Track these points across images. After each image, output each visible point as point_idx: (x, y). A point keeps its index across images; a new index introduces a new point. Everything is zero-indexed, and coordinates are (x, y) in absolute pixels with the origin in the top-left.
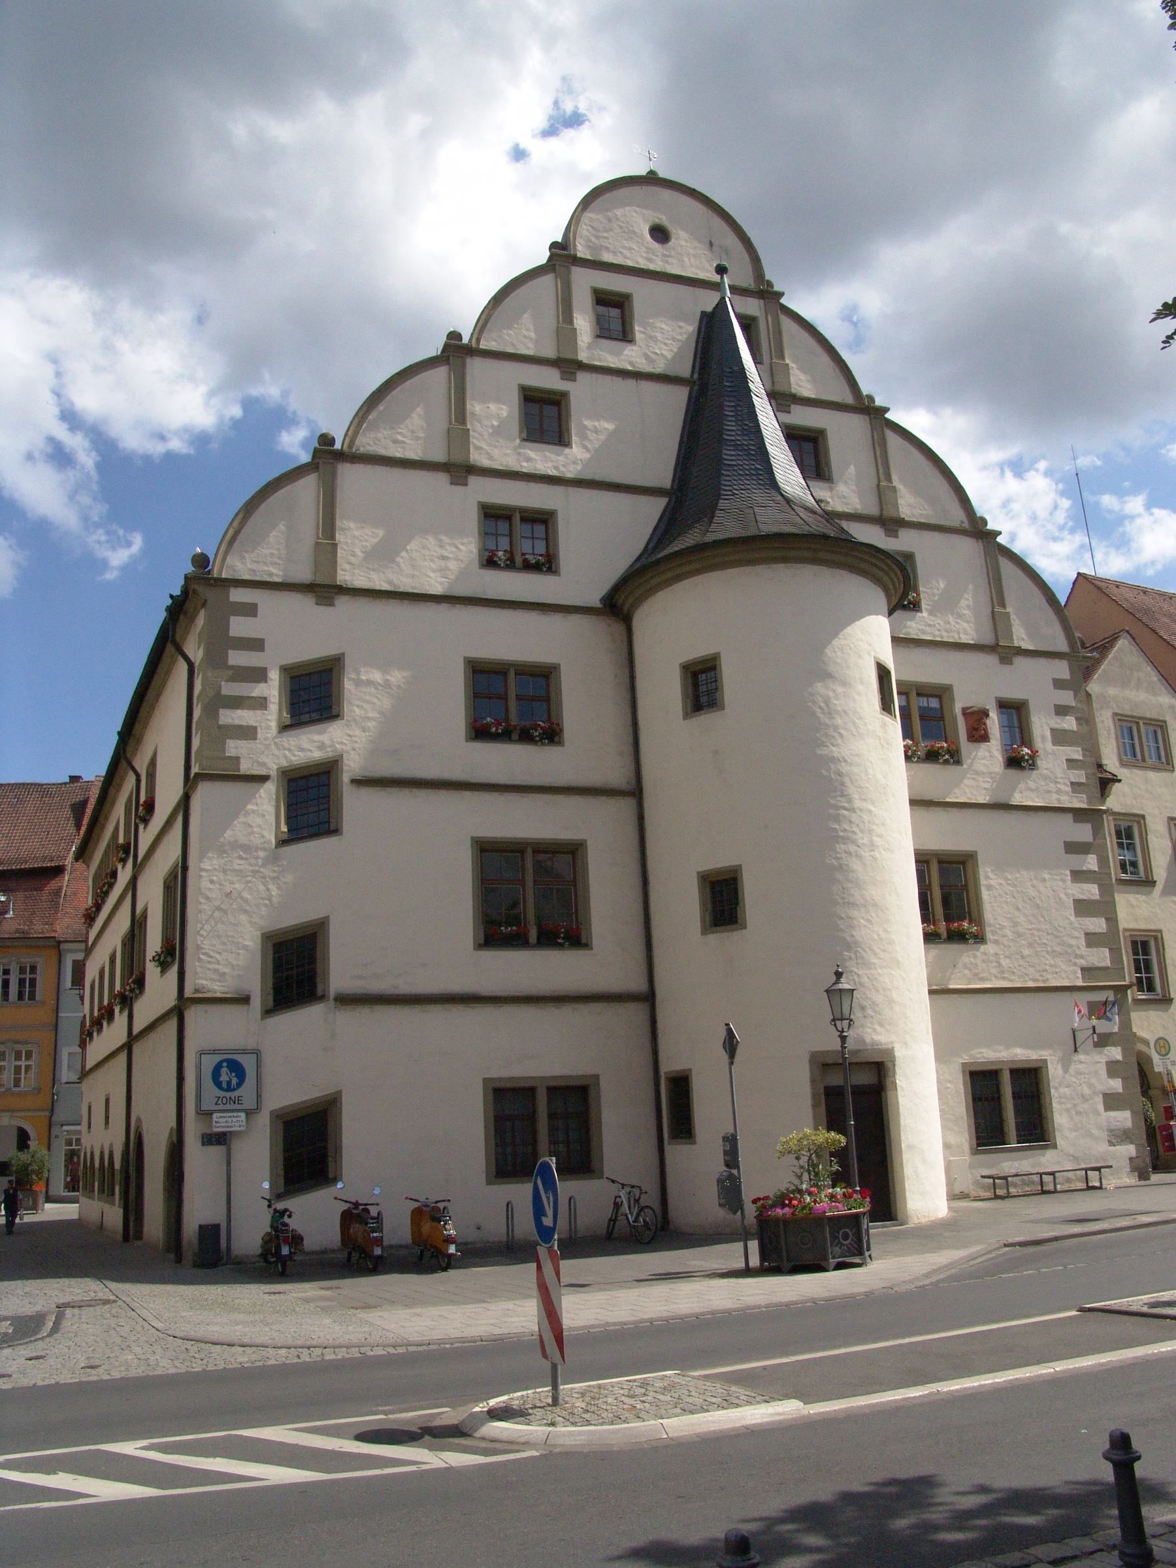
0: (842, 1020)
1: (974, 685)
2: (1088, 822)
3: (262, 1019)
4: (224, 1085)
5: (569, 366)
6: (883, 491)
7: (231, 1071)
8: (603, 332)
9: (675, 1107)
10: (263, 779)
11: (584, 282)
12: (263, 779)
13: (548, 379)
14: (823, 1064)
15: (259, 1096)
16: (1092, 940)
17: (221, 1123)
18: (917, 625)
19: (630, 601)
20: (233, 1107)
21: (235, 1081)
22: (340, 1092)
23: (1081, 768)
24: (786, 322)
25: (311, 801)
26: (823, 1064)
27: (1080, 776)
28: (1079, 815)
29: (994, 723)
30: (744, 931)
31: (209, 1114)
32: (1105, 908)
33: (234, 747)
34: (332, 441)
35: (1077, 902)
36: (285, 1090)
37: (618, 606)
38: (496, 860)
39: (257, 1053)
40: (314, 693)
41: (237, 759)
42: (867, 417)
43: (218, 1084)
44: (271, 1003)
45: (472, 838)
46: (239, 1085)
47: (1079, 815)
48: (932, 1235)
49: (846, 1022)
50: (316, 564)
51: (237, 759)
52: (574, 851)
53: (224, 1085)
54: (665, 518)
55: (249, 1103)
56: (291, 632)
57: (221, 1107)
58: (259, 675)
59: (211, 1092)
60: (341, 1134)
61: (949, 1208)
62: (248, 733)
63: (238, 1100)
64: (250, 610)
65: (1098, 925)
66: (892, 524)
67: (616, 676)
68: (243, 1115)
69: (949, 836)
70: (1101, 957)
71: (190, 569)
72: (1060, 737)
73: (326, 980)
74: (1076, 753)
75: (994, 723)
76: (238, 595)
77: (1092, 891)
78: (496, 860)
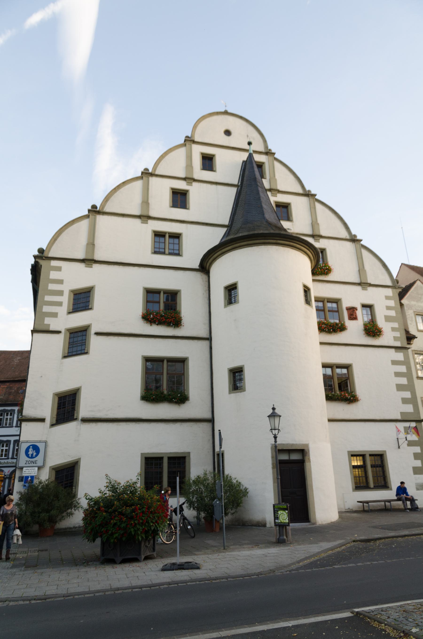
0: (275, 430)
2: (401, 352)
3: (50, 428)
4: (30, 456)
5: (189, 179)
6: (314, 224)
10: (59, 332)
11: (197, 151)
12: (59, 332)
13: (181, 185)
15: (44, 460)
16: (405, 401)
19: (208, 264)
20: (33, 465)
21: (35, 454)
22: (80, 459)
23: (399, 341)
24: (276, 164)
27: (398, 334)
29: (359, 313)
30: (245, 392)
33: (47, 320)
34: (96, 208)
35: (394, 337)
39: (46, 442)
40: (82, 300)
41: (49, 325)
42: (308, 198)
43: (27, 455)
44: (54, 422)
45: (142, 356)
46: (36, 456)
49: (277, 431)
50: (87, 252)
51: (49, 325)
52: (183, 361)
53: (30, 456)
56: (74, 277)
57: (28, 465)
58: (60, 293)
60: (79, 476)
61: (339, 516)
62: (55, 315)
63: (35, 462)
64: (59, 269)
65: (407, 395)
66: (317, 236)
67: (203, 294)
68: (36, 468)
73: (78, 413)
74: (396, 325)
76: (54, 263)
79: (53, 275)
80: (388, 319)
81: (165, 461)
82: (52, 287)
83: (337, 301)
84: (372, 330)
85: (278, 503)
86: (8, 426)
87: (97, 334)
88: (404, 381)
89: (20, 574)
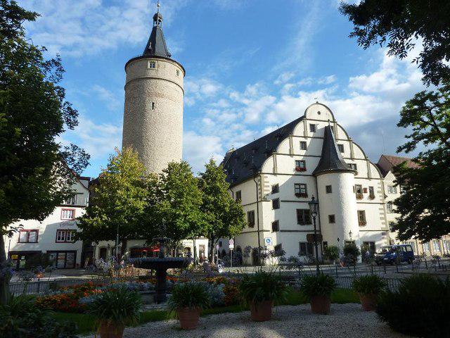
1: (366, 184)
8: (305, 143)
13: (303, 140)
25: (276, 205)
29: (368, 191)
32: (385, 218)
38: (299, 212)
65: (384, 221)
70: (384, 226)
71: (348, 16)
72: (378, 192)
74: (381, 194)
75: (368, 191)
78: (299, 212)
79: (265, 180)
80: (378, 192)
82: (266, 184)
83: (360, 186)
84: (372, 197)
85: (203, 86)
86: (71, 204)
88: (383, 216)
89: (362, 215)
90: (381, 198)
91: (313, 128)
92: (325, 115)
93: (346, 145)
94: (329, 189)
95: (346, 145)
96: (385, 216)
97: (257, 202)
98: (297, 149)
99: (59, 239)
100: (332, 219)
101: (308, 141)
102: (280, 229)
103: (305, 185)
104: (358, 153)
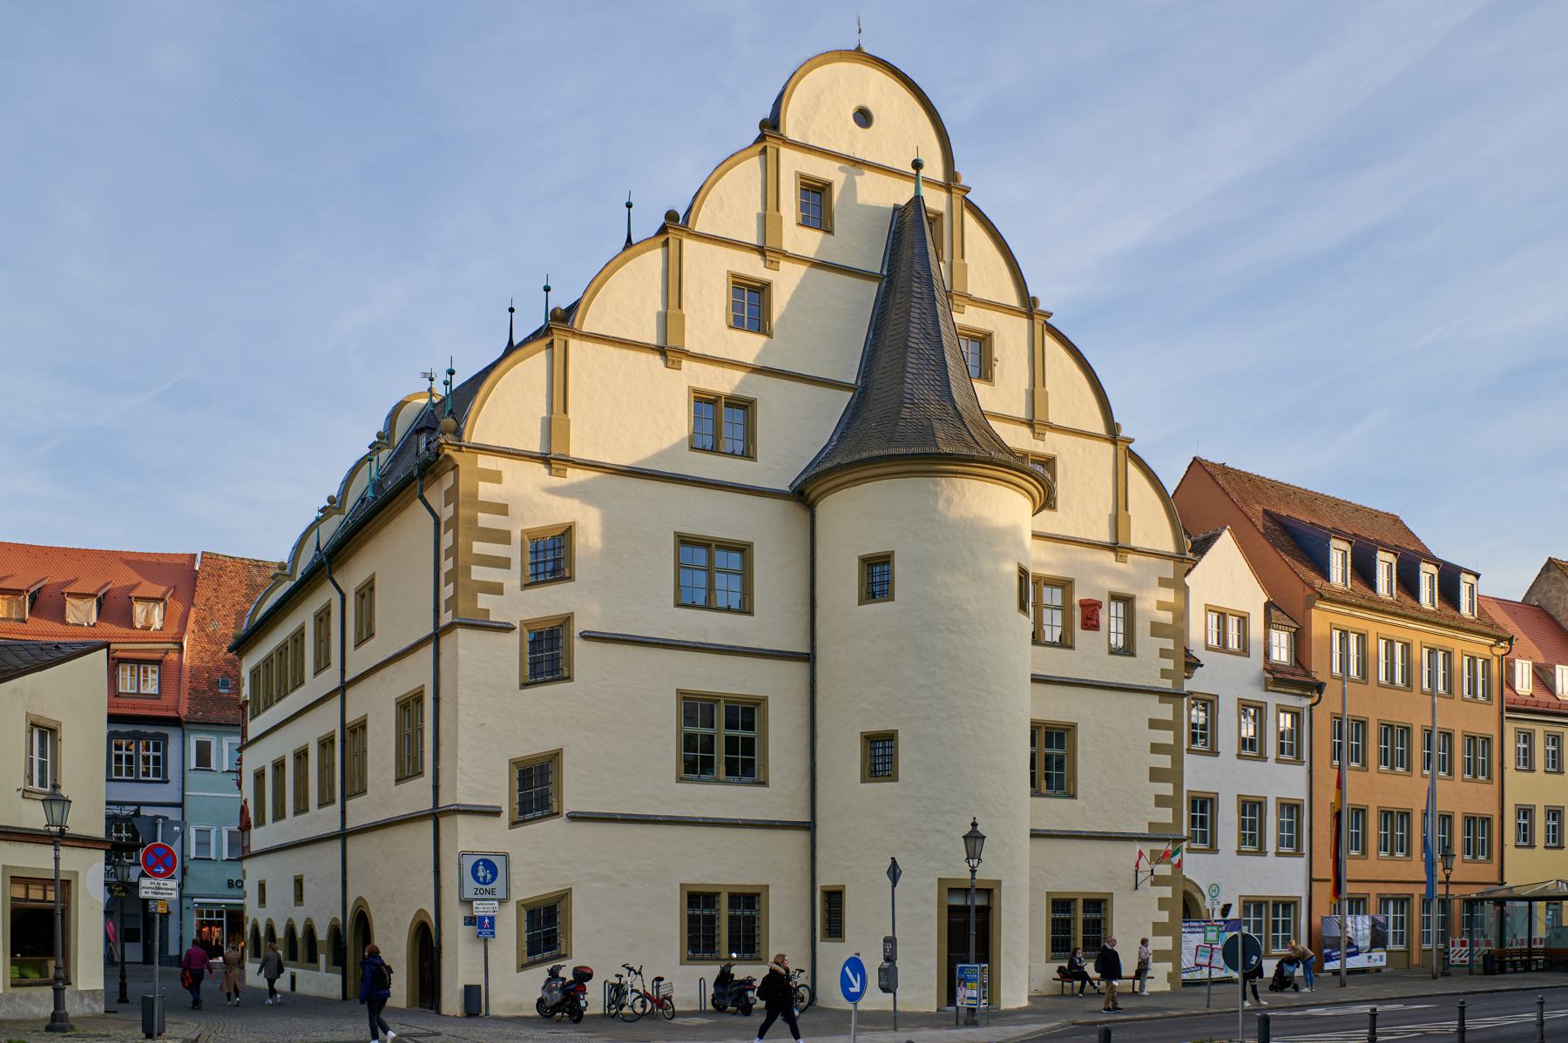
7: (487, 869)
9: (831, 912)
10: (507, 628)
12: (507, 628)
13: (752, 266)
14: (950, 888)
15: (508, 889)
16: (1161, 801)
17: (480, 909)
18: (1049, 522)
25: (547, 654)
26: (950, 888)
28: (1164, 695)
31: (469, 902)
32: (1174, 775)
36: (528, 884)
37: (804, 495)
39: (506, 856)
43: (477, 879)
46: (493, 880)
47: (1164, 695)
48: (1014, 1016)
54: (848, 415)
55: (500, 894)
59: (471, 885)
62: (496, 589)
63: (492, 892)
64: (496, 477)
65: (1167, 789)
69: (1059, 707)
70: (1165, 815)
74: (1169, 644)
76: (485, 462)
77: (1165, 761)
81: (973, 911)
87: (588, 636)
88: (1165, 761)
90: (1169, 664)
91: (815, 195)
92: (902, 133)
93: (1011, 336)
94: (877, 576)
95: (1011, 336)
96: (1178, 762)
97: (436, 636)
98: (707, 321)
99: (118, 772)
100: (880, 756)
101: (785, 282)
102: (568, 806)
103: (744, 549)
104: (1069, 399)
